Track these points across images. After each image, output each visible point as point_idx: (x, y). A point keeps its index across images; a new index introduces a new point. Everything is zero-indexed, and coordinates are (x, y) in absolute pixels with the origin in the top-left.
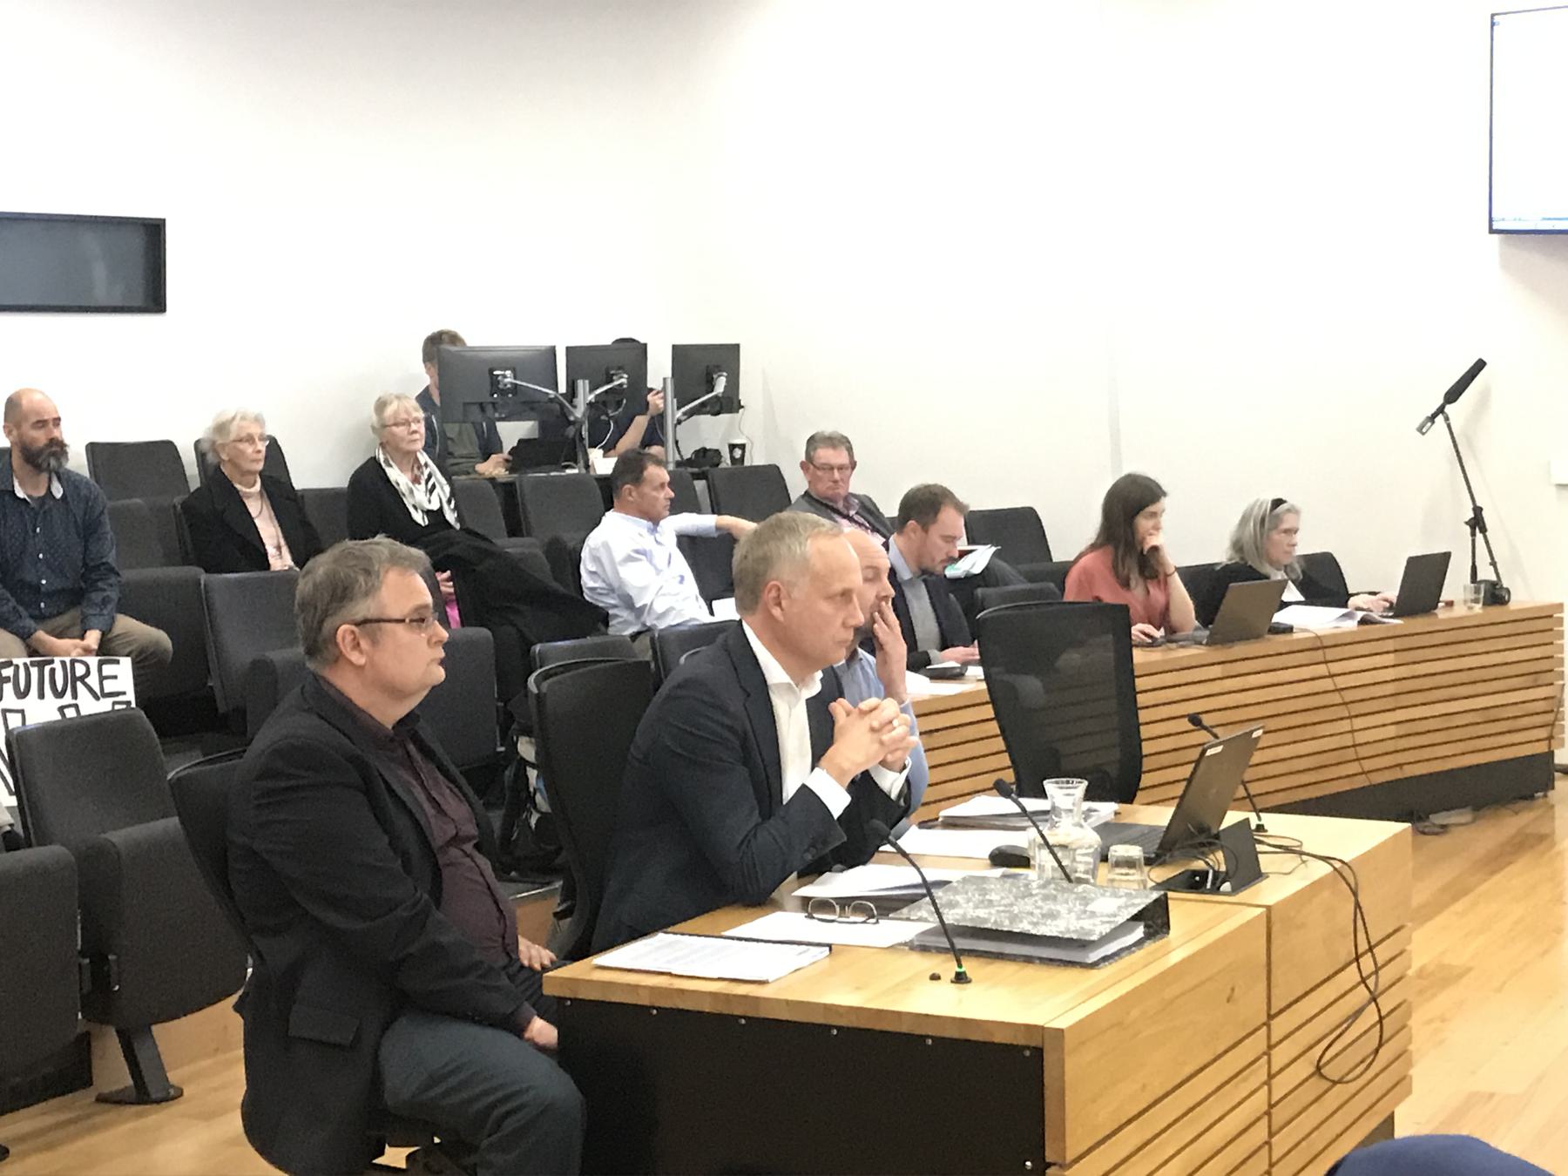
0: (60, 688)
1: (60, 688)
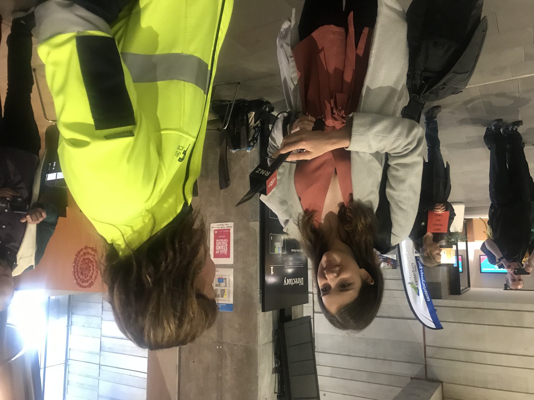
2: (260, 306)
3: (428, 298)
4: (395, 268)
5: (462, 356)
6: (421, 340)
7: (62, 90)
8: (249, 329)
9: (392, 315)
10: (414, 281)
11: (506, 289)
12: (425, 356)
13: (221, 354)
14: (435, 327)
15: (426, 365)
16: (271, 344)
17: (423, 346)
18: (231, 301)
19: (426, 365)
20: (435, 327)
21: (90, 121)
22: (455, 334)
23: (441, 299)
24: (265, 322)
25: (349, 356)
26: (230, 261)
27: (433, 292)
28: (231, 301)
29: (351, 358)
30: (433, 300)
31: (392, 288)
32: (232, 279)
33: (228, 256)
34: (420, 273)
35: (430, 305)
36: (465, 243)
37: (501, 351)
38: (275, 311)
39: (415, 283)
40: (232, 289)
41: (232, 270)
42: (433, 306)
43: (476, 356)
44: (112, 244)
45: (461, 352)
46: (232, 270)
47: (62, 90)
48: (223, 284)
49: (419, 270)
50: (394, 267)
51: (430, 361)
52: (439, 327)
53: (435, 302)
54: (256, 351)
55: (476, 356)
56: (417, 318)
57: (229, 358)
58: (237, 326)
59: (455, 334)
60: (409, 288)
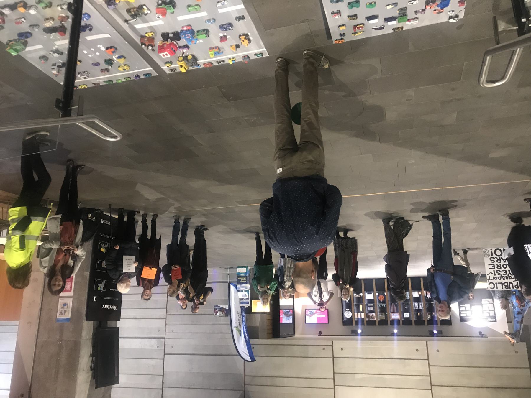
0: (511, 285)
1: (511, 285)
2: (85, 318)
3: (247, 338)
4: (227, 316)
5: (269, 381)
6: (242, 372)
7: (15, 242)
8: (78, 331)
9: (223, 353)
10: (239, 325)
11: (320, 335)
12: (244, 385)
13: (60, 347)
14: (250, 360)
15: (244, 391)
16: (91, 341)
17: (243, 376)
18: (69, 316)
19: (244, 391)
20: (250, 360)
21: (19, 247)
22: (265, 365)
23: (258, 339)
24: (87, 328)
25: (189, 388)
26: (71, 294)
27: (252, 333)
28: (69, 316)
29: (190, 390)
30: (250, 340)
31: (224, 332)
32: (71, 304)
33: (70, 291)
34: (243, 318)
35: (248, 343)
36: (292, 299)
37: (294, 376)
38: (96, 322)
39: (239, 327)
40: (70, 309)
41: (72, 299)
42: (250, 345)
43: (278, 381)
44: (279, 157)
45: (268, 379)
46: (72, 299)
47: (15, 242)
48: (66, 307)
49: (243, 316)
50: (227, 316)
51: (248, 388)
52: (253, 360)
53: (252, 341)
54: (80, 343)
55: (278, 381)
56: (240, 355)
57: (65, 348)
58: (71, 330)
59: (265, 365)
60: (235, 330)
